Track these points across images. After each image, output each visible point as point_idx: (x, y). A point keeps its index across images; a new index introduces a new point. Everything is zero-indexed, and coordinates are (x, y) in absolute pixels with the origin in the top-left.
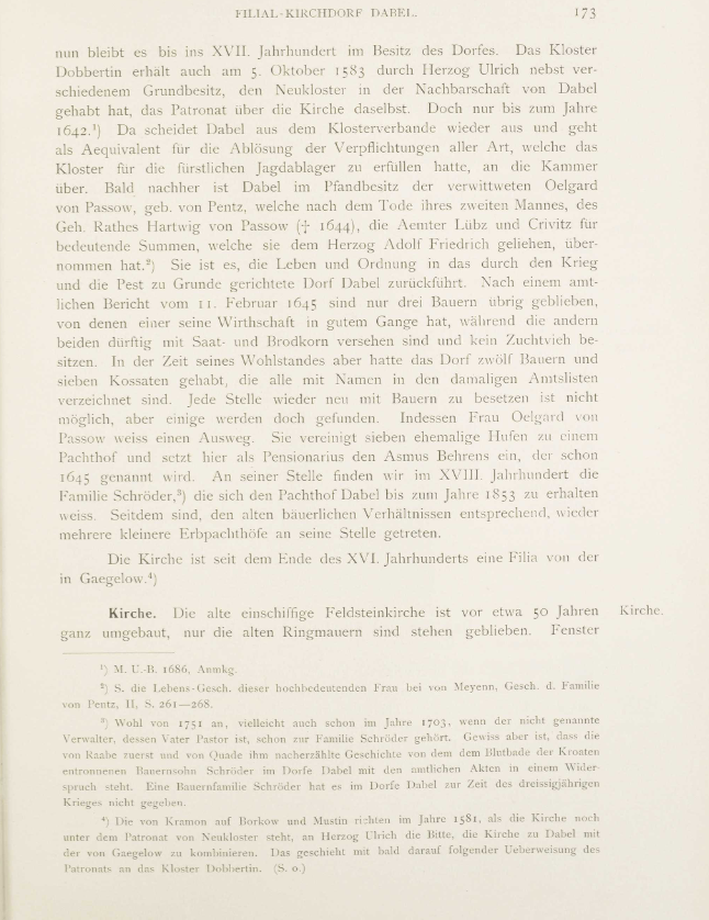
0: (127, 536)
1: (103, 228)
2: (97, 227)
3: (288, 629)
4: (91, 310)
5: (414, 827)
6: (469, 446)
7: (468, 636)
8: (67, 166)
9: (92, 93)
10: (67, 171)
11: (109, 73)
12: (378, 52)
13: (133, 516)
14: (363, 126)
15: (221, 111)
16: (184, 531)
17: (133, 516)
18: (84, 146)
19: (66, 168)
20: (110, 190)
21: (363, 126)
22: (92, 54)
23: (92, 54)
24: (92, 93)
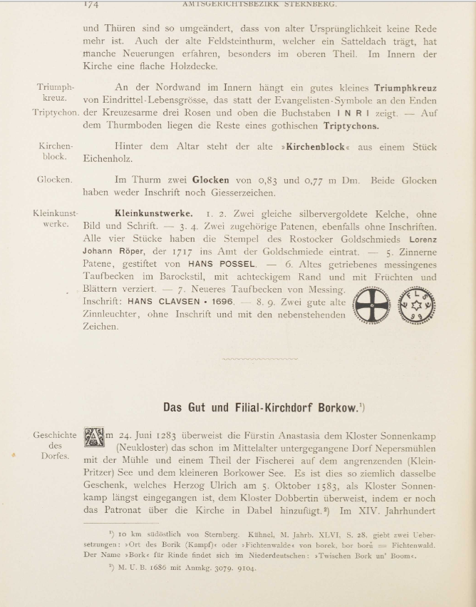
0: (184, 474)
1: (305, 277)
2: (292, 239)
3: (220, 123)
4: (434, 104)
5: (221, 94)
6: (331, 271)
7: (274, 129)
8: (353, 434)
9: (128, 193)
10: (353, 437)
11: (310, 499)
12: (374, 182)
13: (290, 499)
14: (388, 485)
15: (394, 499)
16: (106, 98)
17: (290, 499)
18: (136, 38)
19: (371, 486)
20: (163, 277)
21: (388, 485)
22: (45, 157)
23: (45, 157)
24: (128, 193)
